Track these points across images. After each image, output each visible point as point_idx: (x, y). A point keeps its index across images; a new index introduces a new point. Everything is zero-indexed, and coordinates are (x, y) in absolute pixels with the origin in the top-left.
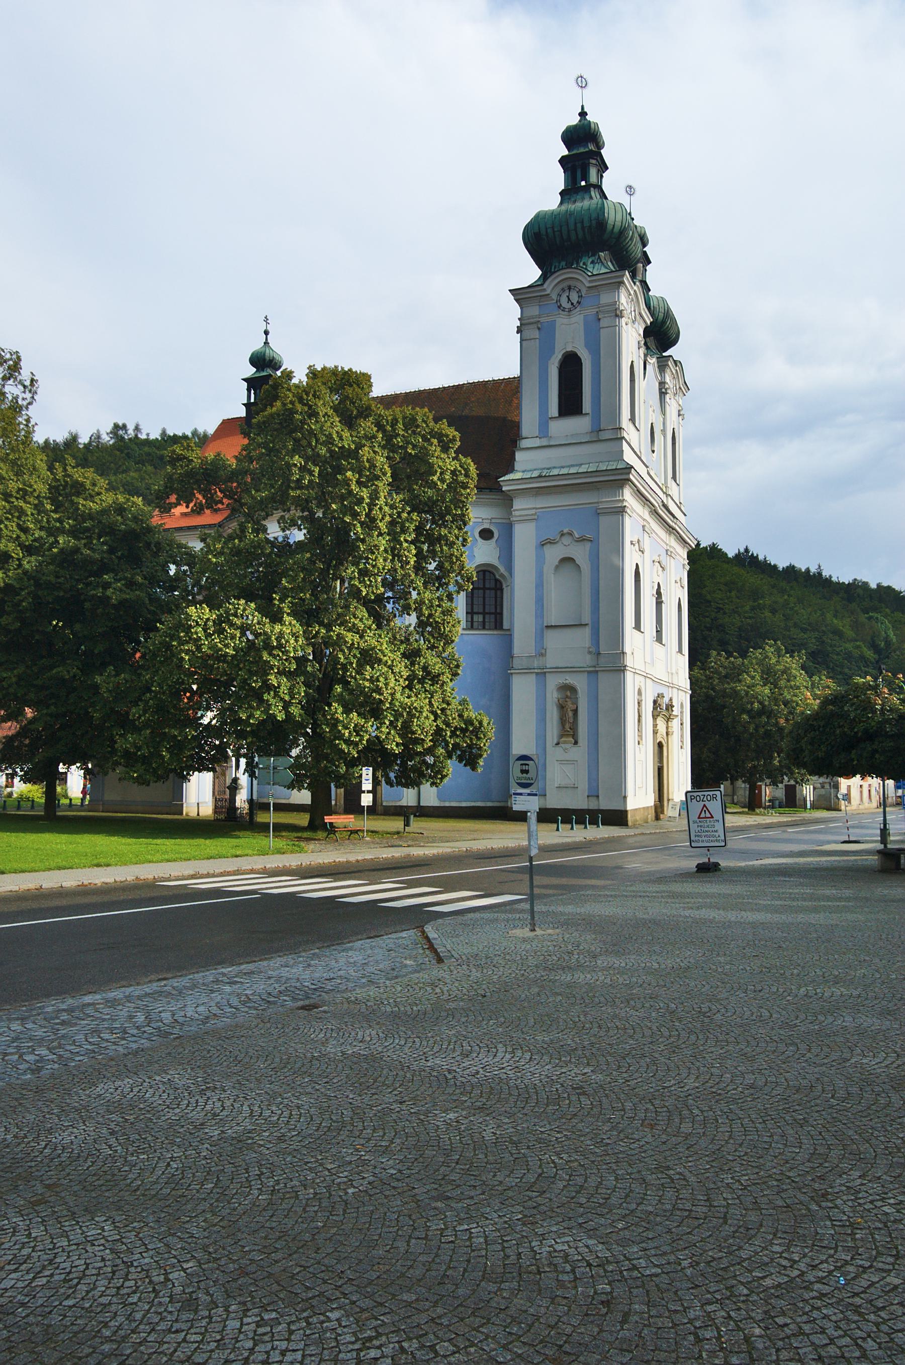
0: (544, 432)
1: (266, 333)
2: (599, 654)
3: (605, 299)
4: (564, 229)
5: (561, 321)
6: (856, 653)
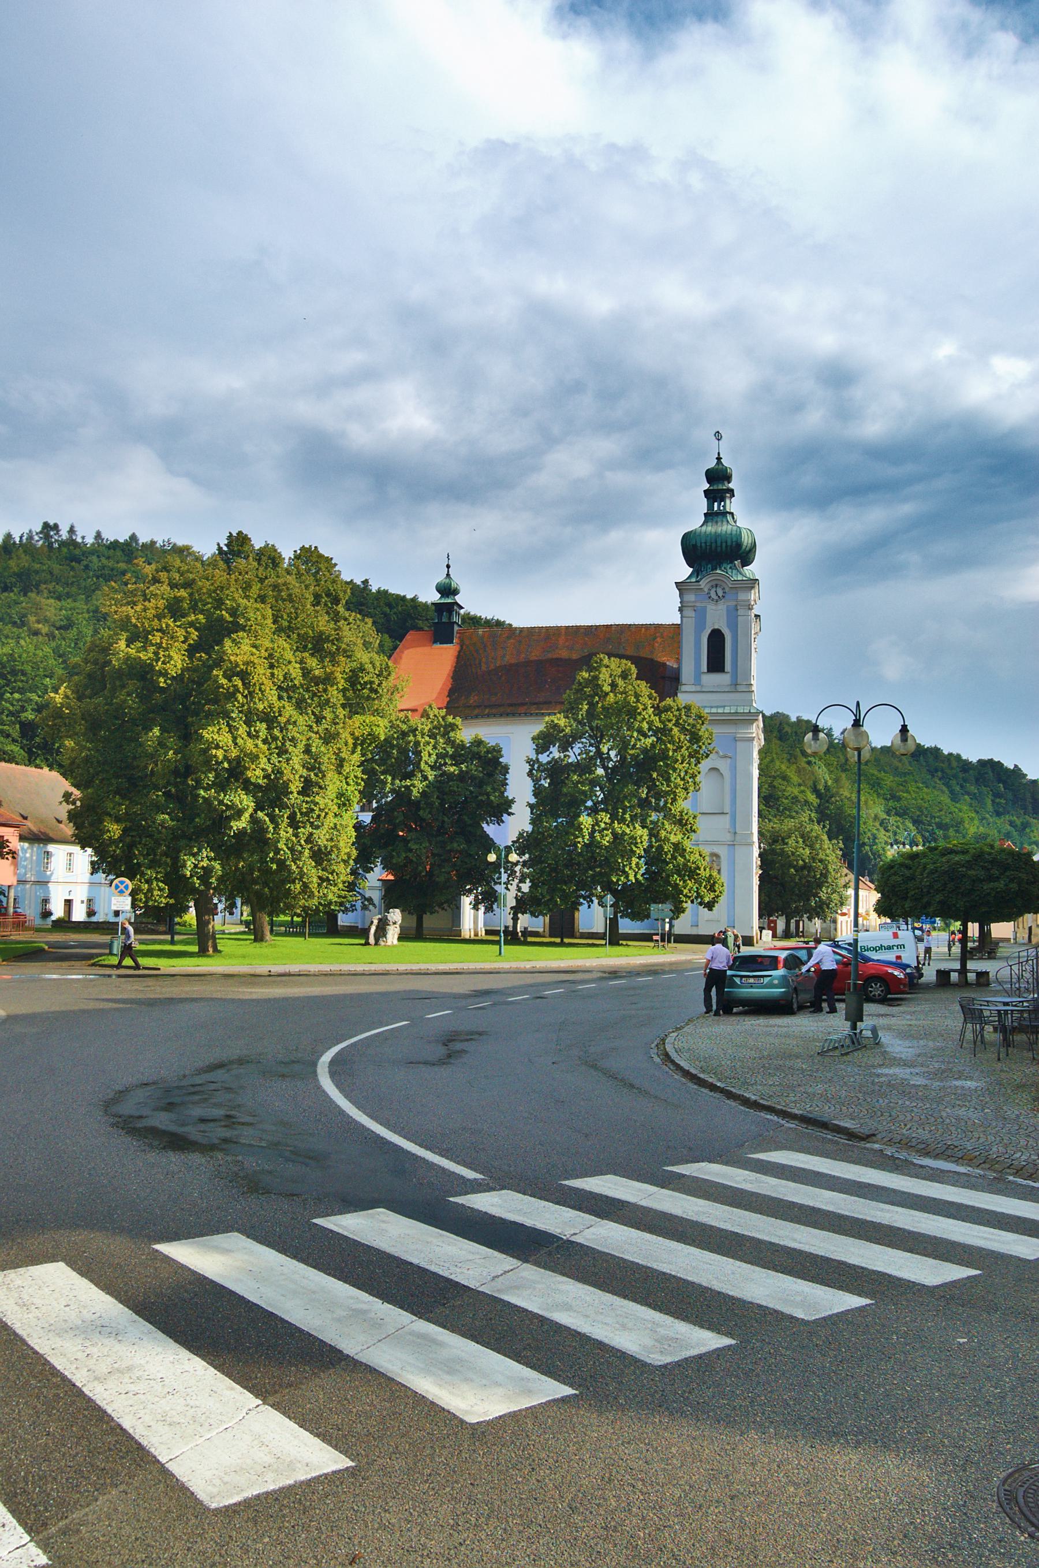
0: (698, 681)
1: (448, 566)
2: (735, 833)
3: (742, 596)
4: (714, 545)
5: (711, 607)
6: (801, 797)
